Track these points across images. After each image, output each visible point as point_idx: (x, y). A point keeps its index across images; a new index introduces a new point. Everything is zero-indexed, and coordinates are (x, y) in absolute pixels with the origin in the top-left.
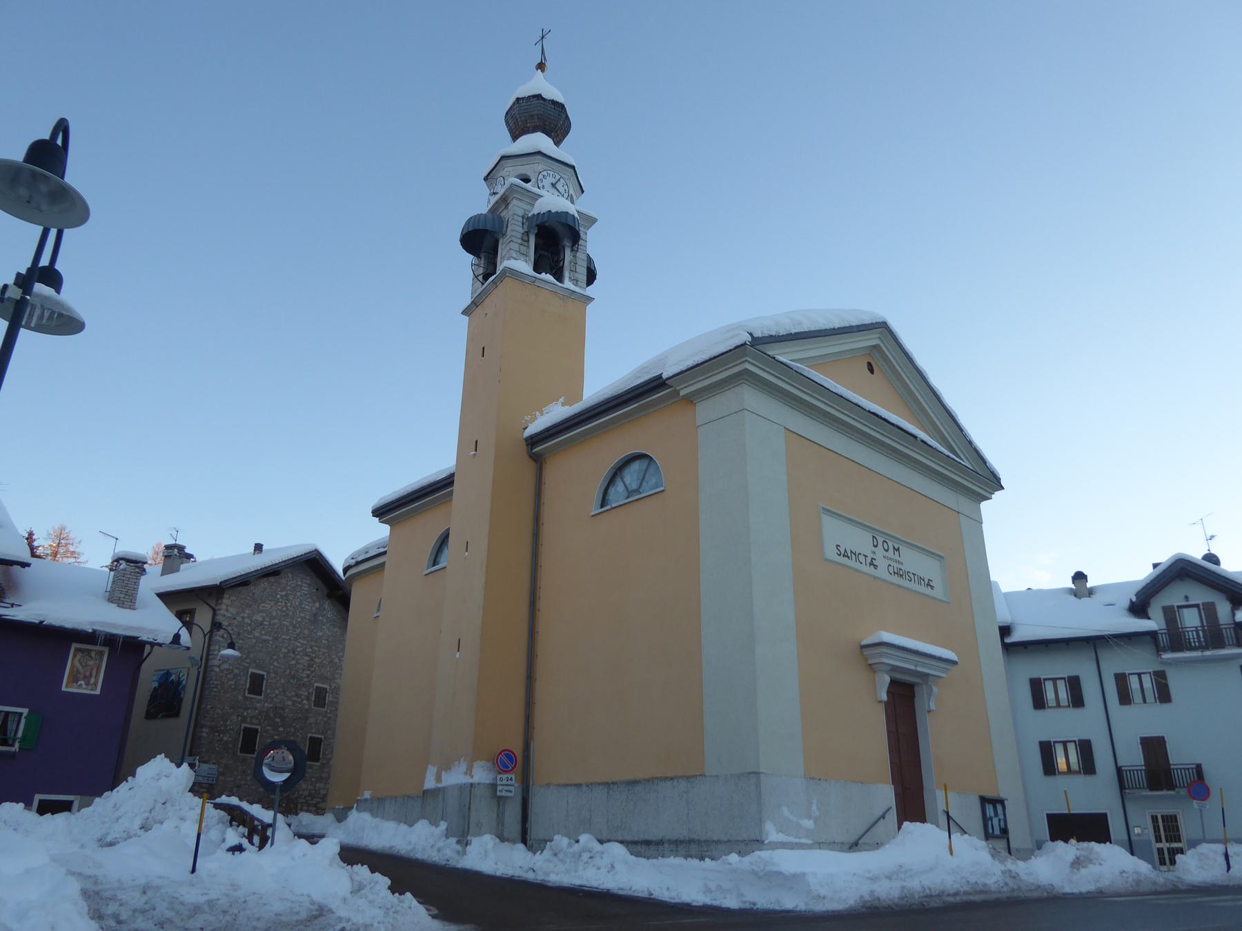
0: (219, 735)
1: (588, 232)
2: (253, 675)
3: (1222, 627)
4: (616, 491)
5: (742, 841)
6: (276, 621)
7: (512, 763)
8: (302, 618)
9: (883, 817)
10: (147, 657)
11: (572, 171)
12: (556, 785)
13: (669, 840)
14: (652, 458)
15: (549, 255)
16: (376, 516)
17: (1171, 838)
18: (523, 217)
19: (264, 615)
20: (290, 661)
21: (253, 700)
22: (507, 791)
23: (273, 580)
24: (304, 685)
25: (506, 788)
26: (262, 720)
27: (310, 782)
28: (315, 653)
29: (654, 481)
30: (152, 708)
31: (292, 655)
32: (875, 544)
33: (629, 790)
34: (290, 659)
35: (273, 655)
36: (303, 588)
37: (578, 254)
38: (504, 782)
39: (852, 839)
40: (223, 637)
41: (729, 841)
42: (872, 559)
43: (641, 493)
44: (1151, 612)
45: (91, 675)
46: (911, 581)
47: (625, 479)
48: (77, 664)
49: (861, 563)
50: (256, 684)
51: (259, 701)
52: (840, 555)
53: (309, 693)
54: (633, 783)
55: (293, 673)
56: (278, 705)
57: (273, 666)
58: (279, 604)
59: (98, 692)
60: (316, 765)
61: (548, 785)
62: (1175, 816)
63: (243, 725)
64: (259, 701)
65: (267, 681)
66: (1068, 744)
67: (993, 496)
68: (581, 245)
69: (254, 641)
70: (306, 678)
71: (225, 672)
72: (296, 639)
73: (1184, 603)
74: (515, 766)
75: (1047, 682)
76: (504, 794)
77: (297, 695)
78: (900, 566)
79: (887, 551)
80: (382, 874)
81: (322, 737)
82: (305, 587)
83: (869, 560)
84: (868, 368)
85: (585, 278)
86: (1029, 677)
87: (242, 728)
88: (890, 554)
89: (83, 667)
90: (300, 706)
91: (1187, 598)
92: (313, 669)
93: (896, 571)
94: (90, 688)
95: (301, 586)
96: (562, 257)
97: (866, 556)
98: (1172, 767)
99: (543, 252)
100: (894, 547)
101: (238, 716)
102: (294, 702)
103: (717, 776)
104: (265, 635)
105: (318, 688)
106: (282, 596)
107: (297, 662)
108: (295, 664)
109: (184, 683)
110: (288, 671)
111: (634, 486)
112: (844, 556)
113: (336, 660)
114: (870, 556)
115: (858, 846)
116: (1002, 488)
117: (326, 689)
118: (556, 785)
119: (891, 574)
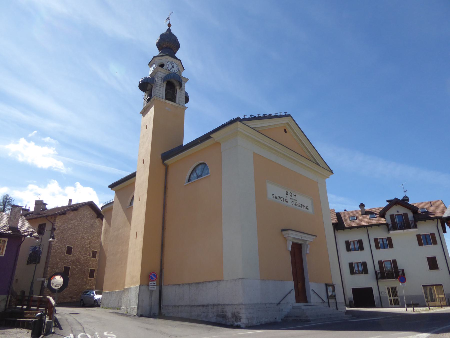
0: (55, 270)
1: (186, 84)
2: (68, 247)
3: (410, 221)
4: (193, 176)
6: (77, 227)
8: (87, 226)
9: (290, 293)
10: (23, 241)
11: (180, 62)
12: (171, 285)
13: (211, 305)
14: (206, 164)
15: (171, 92)
16: (110, 188)
17: (396, 303)
18: (161, 78)
19: (72, 225)
20: (82, 241)
21: (68, 256)
22: (153, 288)
23: (76, 212)
24: (88, 250)
25: (153, 287)
26: (71, 264)
27: (90, 286)
28: (92, 238)
29: (206, 172)
30: (30, 260)
31: (83, 240)
32: (287, 194)
34: (82, 241)
35: (76, 240)
36: (87, 215)
37: (182, 92)
38: (152, 284)
39: (277, 302)
40: (56, 234)
41: (232, 304)
43: (202, 177)
44: (386, 216)
46: (300, 207)
47: (196, 172)
50: (69, 250)
51: (71, 257)
52: (274, 198)
53: (89, 253)
54: (198, 283)
55: (83, 246)
56: (78, 258)
57: (76, 243)
58: (78, 221)
59: (3, 255)
60: (93, 280)
61: (169, 285)
62: (395, 288)
63: (64, 266)
64: (71, 257)
65: (73, 249)
67: (330, 176)
69: (68, 235)
70: (89, 248)
71: (57, 246)
72: (85, 234)
73: (397, 214)
74: (156, 278)
75: (351, 242)
76: (152, 289)
77: (85, 254)
78: (296, 202)
81: (95, 269)
82: (88, 214)
83: (285, 200)
84: (285, 131)
85: (184, 100)
87: (64, 267)
88: (293, 197)
90: (86, 258)
91: (398, 212)
92: (91, 244)
93: (295, 203)
95: (87, 214)
96: (176, 92)
97: (283, 198)
99: (169, 91)
100: (294, 195)
101: (62, 262)
102: (84, 257)
104: (73, 232)
105: (93, 251)
106: (79, 218)
107: (85, 242)
108: (84, 243)
109: (41, 251)
110: (82, 245)
111: (200, 174)
112: (275, 198)
114: (285, 198)
115: (280, 304)
117: (96, 251)
118: (171, 285)
119: (293, 204)
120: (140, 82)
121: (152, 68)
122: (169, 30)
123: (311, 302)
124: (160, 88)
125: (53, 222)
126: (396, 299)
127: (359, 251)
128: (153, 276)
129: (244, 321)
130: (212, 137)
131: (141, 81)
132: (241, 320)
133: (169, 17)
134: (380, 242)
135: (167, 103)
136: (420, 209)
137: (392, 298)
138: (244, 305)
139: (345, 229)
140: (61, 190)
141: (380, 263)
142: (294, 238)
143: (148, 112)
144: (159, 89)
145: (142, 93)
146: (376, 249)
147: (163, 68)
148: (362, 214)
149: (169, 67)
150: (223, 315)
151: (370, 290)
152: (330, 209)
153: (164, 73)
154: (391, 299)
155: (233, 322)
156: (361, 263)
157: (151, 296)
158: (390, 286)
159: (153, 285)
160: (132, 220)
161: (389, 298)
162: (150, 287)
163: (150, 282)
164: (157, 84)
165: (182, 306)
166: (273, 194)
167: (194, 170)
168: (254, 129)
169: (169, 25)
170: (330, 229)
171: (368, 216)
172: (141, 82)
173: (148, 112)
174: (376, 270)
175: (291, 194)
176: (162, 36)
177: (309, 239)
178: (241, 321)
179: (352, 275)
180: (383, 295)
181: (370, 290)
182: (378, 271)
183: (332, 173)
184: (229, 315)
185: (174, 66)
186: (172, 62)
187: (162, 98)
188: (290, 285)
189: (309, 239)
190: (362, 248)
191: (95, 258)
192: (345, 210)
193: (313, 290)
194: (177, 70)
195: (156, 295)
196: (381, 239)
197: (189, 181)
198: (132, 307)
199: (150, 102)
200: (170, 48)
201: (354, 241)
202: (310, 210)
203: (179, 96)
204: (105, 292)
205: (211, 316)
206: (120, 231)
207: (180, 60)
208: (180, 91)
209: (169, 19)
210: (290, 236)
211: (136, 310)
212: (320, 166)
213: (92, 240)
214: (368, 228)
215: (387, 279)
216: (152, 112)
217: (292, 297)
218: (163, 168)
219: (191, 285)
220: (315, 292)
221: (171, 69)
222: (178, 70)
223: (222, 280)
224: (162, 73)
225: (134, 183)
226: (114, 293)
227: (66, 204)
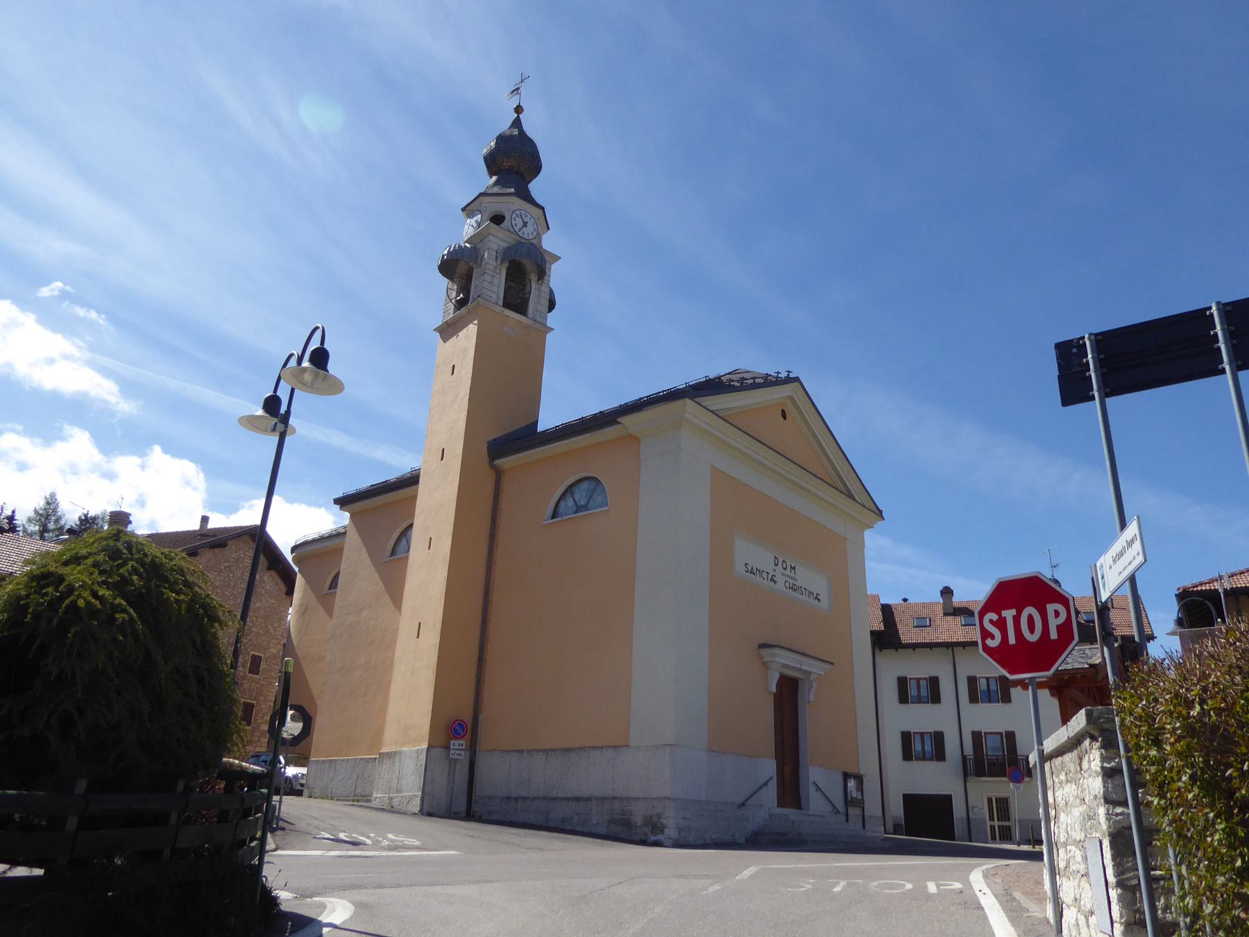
5: (656, 799)
7: (454, 728)
9: (766, 784)
14: (599, 481)
22: (458, 754)
25: (458, 752)
29: (600, 499)
33: (564, 757)
36: (245, 560)
39: (740, 800)
42: (773, 575)
47: (574, 496)
49: (764, 579)
52: (747, 572)
54: (569, 750)
58: (222, 574)
61: (493, 750)
66: (925, 735)
76: (456, 757)
79: (785, 569)
80: (798, 689)
83: (770, 577)
88: (788, 572)
92: (249, 638)
96: (528, 290)
97: (768, 573)
98: (1019, 757)
103: (639, 747)
105: (253, 656)
106: (225, 567)
111: (583, 503)
112: (751, 572)
113: (272, 630)
114: (771, 573)
117: (261, 657)
120: (443, 256)
121: (473, 221)
122: (517, 123)
123: (808, 809)
124: (493, 277)
126: (1006, 826)
127: (928, 705)
129: (671, 832)
130: (619, 423)
131: (447, 255)
132: (665, 830)
133: (519, 88)
134: (982, 685)
135: (506, 316)
136: (1084, 613)
137: (996, 823)
138: (675, 800)
139: (900, 648)
140: (97, 456)
141: (977, 736)
142: (785, 666)
143: (460, 334)
145: (444, 281)
146: (970, 702)
147: (501, 226)
148: (945, 614)
149: (516, 225)
150: (623, 819)
151: (946, 800)
152: (869, 593)
153: (503, 240)
154: (994, 826)
155: (646, 834)
156: (931, 733)
157: (451, 774)
158: (993, 794)
159: (459, 747)
160: (405, 593)
161: (989, 823)
162: (452, 752)
163: (452, 742)
164: (488, 266)
165: (525, 798)
166: (746, 564)
167: (569, 490)
168: (716, 413)
169: (519, 109)
170: (863, 644)
171: (958, 618)
172: (445, 257)
173: (460, 331)
174: (966, 753)
175: (784, 563)
176: (501, 139)
178: (663, 834)
179: (906, 762)
180: (975, 814)
181: (946, 800)
182: (970, 757)
183: (880, 518)
184: (639, 821)
185: (527, 222)
187: (497, 304)
188: (769, 767)
190: (935, 698)
191: (258, 674)
192: (905, 600)
194: (535, 233)
195: (462, 772)
196: (985, 679)
197: (553, 517)
198: (405, 794)
199: (464, 310)
200: (517, 173)
201: (918, 680)
202: (825, 603)
203: (536, 301)
204: (318, 760)
205: (595, 822)
206: (364, 614)
207: (543, 209)
209: (519, 91)
210: (777, 659)
211: (417, 801)
212: (857, 502)
213: (253, 627)
214: (955, 648)
215: (989, 776)
216: (469, 334)
217: (772, 791)
218: (490, 477)
219: (550, 753)
220: (818, 789)
221: (520, 230)
223: (627, 746)
224: (498, 240)
225: (414, 498)
226: (344, 762)
227: (196, 526)
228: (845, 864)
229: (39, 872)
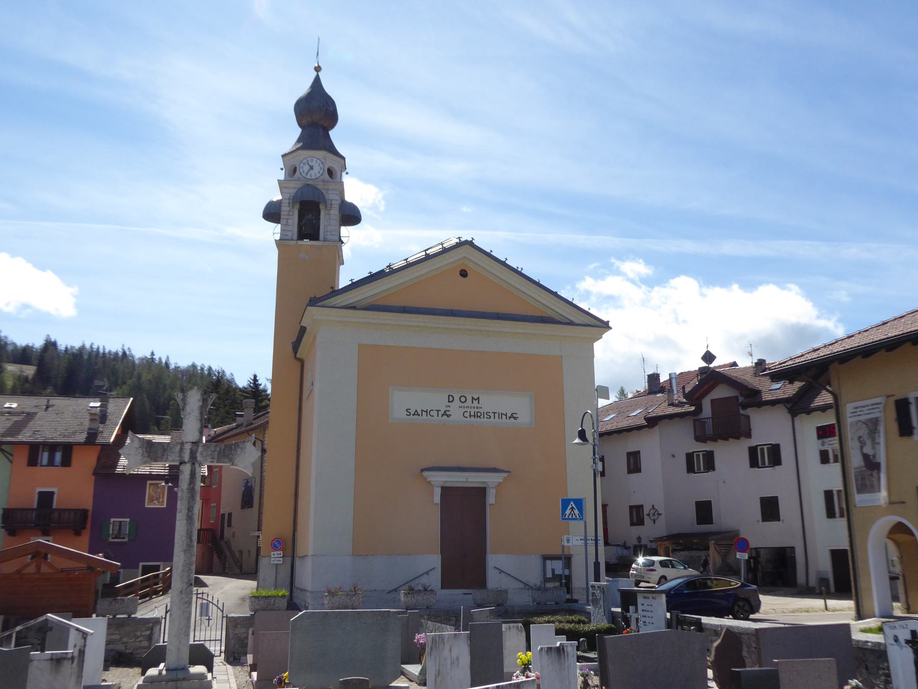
18: (289, 199)
38: (276, 556)
45: (160, 498)
48: (151, 492)
59: (165, 506)
68: (334, 204)
86: (686, 452)
89: (155, 493)
94: (160, 504)
116: (611, 328)
125: (262, 439)
128: (276, 543)
144: (285, 223)
162: (272, 559)
177: (490, 480)
186: (309, 159)
189: (490, 480)
193: (495, 567)
208: (326, 213)
222: (322, 170)
228: (69, 549)
229: (733, 669)
